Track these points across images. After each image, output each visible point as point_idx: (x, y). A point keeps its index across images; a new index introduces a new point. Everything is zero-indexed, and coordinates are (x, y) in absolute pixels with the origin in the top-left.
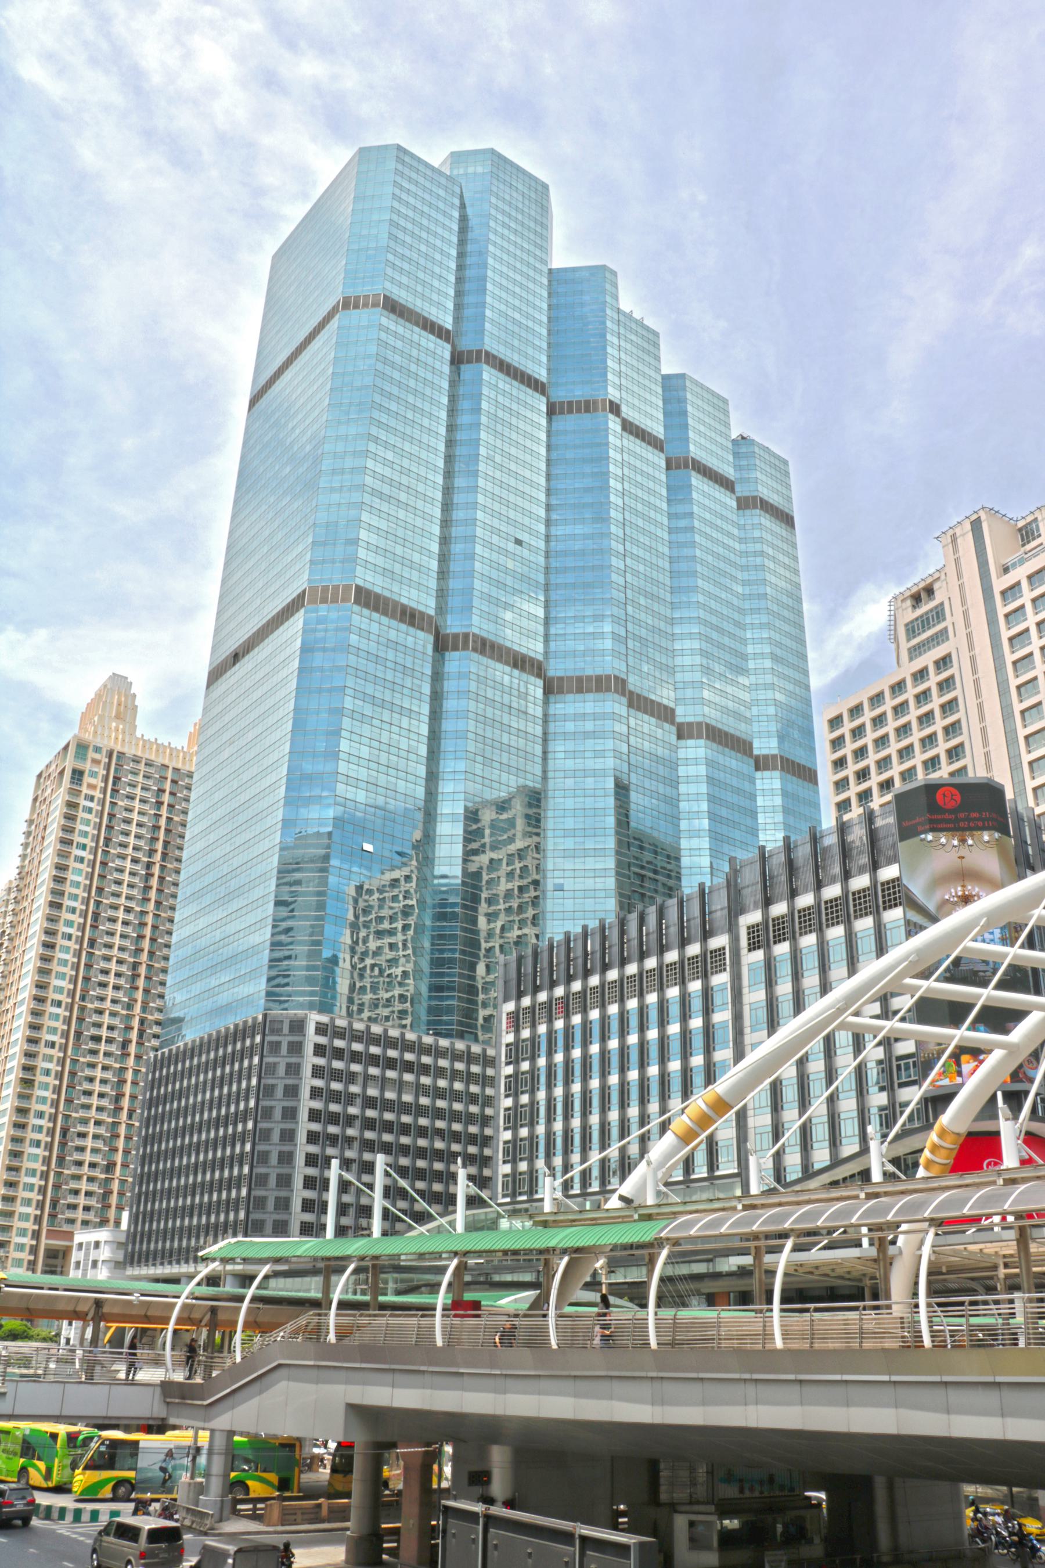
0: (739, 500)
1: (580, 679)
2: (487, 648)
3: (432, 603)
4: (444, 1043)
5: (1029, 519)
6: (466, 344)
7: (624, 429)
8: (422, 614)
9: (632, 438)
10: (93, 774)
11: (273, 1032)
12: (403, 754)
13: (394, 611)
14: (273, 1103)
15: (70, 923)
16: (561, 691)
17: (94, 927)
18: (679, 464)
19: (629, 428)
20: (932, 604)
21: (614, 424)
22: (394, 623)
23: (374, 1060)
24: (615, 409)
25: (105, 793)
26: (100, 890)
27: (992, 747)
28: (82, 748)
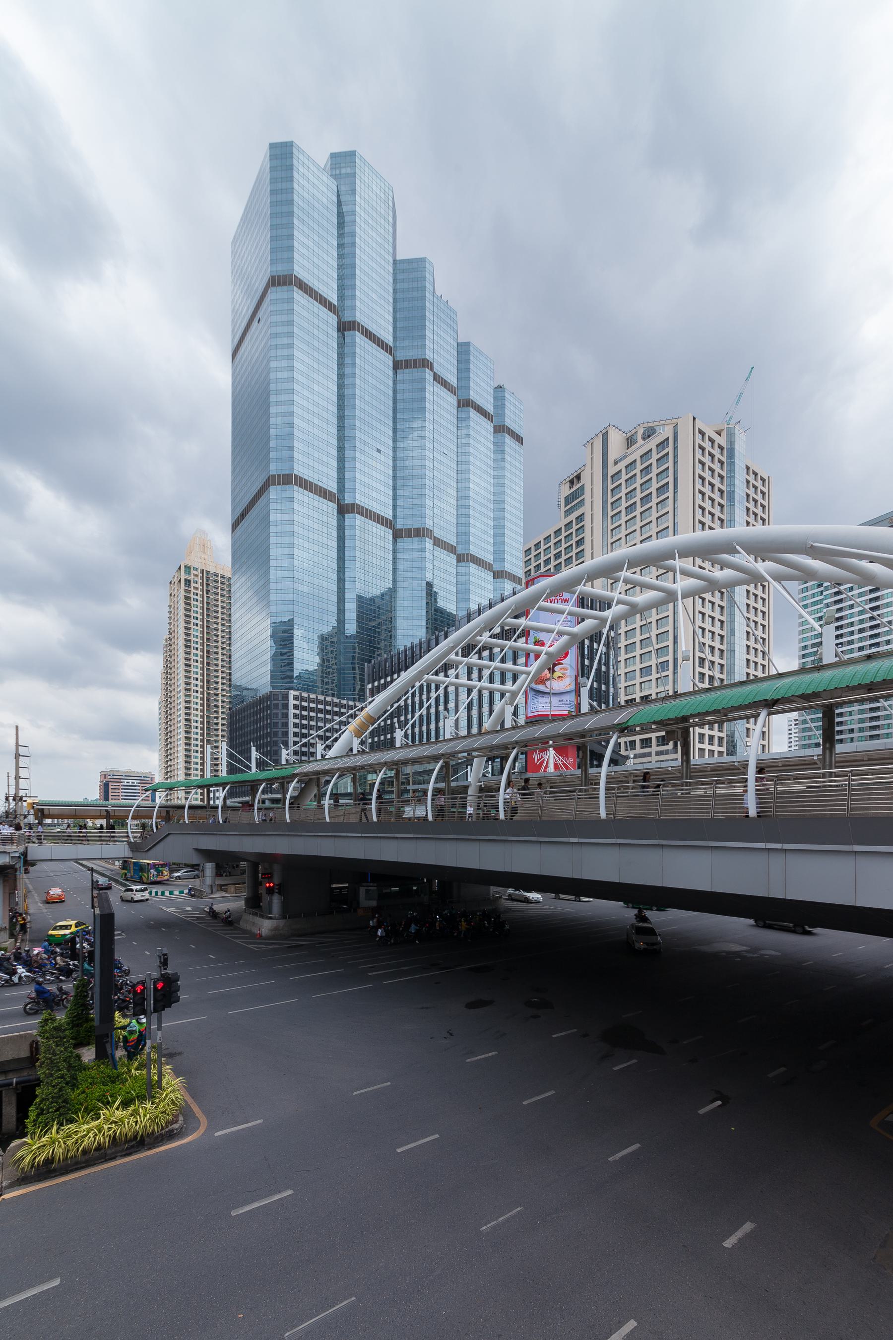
1: (410, 530)
2: (366, 513)
3: (335, 486)
4: (329, 699)
5: (633, 432)
6: (347, 317)
7: (435, 379)
9: (439, 385)
11: (275, 699)
12: (325, 568)
13: (320, 491)
15: (197, 654)
17: (208, 657)
18: (464, 403)
21: (429, 376)
22: (316, 497)
23: (321, 711)
24: (430, 366)
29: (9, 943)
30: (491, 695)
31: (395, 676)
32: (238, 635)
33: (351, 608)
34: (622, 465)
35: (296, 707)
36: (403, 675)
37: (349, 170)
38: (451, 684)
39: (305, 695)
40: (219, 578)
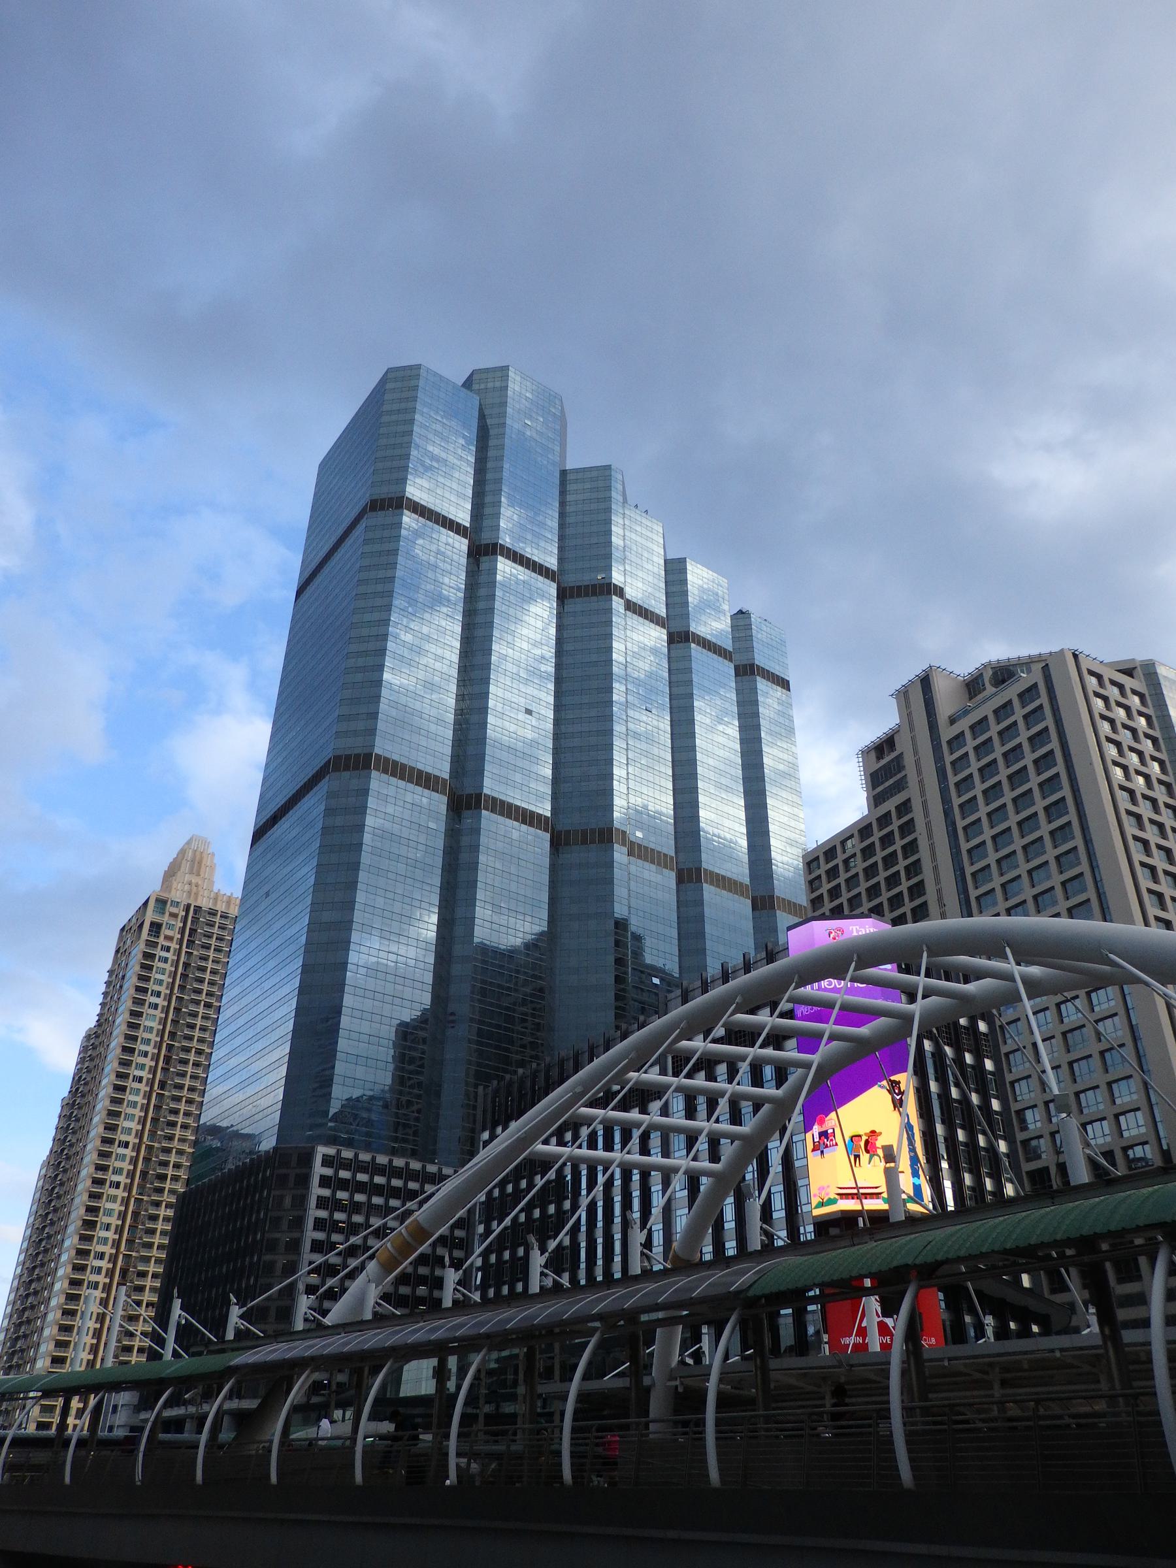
0: (737, 668)
4: (399, 1162)
6: (486, 538)
8: (436, 777)
9: (635, 617)
10: (170, 927)
14: (277, 1235)
15: (143, 1066)
16: (567, 844)
19: (631, 607)
20: (893, 755)
24: (620, 592)
25: (181, 945)
26: (172, 1035)
27: (943, 884)
28: (162, 903)
29: (318, 106)
30: (645, 1176)
31: (499, 1129)
32: (286, 990)
33: (182, 1142)
34: (964, 725)
35: (325, 1182)
36: (513, 1125)
37: (498, 384)
38: (653, 1127)
39: (347, 1154)
40: (217, 919)
